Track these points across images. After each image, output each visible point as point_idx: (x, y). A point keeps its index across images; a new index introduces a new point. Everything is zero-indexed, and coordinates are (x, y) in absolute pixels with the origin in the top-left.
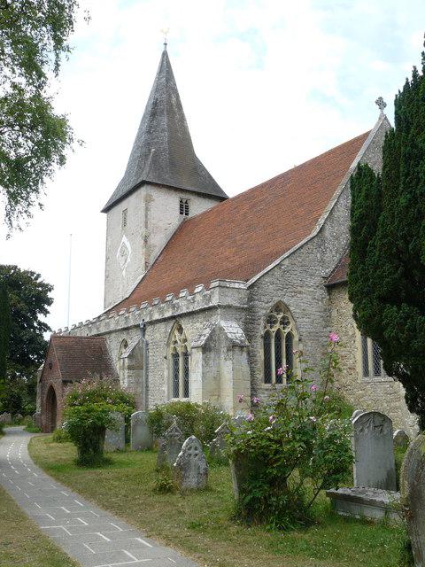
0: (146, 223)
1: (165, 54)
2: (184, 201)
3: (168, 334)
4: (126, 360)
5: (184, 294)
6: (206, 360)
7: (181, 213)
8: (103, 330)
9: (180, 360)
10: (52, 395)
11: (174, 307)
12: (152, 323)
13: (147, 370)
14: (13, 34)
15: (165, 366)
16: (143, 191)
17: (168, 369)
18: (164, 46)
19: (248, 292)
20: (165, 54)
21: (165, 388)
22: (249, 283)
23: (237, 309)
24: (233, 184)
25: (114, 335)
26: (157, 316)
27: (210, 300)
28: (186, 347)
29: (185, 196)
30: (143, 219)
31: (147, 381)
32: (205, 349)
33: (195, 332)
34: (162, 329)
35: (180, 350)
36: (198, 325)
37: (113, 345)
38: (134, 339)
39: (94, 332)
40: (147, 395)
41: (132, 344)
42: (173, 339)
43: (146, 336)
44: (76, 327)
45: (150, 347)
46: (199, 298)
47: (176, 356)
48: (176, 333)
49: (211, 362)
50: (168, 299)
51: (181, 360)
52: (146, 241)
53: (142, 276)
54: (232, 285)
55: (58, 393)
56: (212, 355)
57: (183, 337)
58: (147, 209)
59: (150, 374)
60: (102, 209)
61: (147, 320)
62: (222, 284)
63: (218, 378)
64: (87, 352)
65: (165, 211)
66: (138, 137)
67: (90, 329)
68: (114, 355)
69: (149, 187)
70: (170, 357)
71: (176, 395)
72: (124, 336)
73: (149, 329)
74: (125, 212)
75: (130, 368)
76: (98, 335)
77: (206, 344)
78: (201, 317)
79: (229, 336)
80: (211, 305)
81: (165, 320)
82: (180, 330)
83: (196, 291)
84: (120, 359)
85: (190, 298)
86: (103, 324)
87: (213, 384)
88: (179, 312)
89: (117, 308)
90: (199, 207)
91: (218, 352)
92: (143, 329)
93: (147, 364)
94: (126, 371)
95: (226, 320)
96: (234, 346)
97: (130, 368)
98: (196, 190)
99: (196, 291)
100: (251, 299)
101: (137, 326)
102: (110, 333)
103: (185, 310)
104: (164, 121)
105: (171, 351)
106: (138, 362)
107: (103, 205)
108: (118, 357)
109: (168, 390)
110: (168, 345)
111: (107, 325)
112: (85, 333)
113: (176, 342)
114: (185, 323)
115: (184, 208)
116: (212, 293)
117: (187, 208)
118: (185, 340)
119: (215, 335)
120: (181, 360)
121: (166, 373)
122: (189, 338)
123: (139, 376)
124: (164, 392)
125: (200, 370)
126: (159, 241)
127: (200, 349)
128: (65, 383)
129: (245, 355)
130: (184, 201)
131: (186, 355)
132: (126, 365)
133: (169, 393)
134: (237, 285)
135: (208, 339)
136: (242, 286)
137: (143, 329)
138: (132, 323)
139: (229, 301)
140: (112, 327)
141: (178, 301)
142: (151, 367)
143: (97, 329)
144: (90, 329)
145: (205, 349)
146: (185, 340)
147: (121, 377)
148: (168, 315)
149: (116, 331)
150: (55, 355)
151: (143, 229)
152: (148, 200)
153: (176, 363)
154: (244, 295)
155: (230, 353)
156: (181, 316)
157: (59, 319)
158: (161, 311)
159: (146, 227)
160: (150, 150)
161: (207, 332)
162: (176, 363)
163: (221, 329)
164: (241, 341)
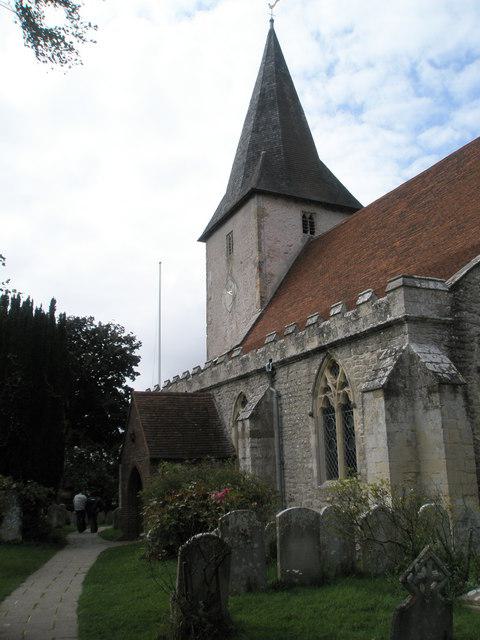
0: (259, 243)
1: (272, 34)
2: (308, 216)
3: (313, 378)
4: (248, 423)
5: (337, 311)
6: (391, 411)
7: (305, 232)
8: (208, 383)
9: (337, 422)
10: (136, 481)
11: (321, 332)
12: (286, 363)
13: (281, 436)
14: (18, 489)
15: (312, 428)
16: (253, 205)
17: (316, 432)
18: (269, 24)
19: (451, 295)
20: (272, 34)
21: (313, 465)
22: (451, 281)
23: (436, 323)
24: (365, 205)
25: (225, 389)
26: (292, 351)
27: (387, 311)
28: (346, 396)
29: (309, 209)
30: (256, 240)
31: (281, 454)
32: (389, 391)
33: (363, 368)
34: (304, 372)
35: (335, 403)
36: (367, 355)
37: (225, 401)
38: (256, 392)
39: (196, 387)
40: (282, 477)
41: (254, 399)
42: (323, 385)
43: (277, 386)
44: (169, 384)
45: (285, 399)
46: (365, 311)
47: (328, 411)
48: (327, 374)
49: (400, 415)
50: (310, 322)
51: (338, 416)
52: (260, 269)
53: (257, 316)
54: (424, 285)
55: (145, 476)
56: (401, 402)
57: (339, 378)
58: (260, 227)
59: (286, 443)
60: (199, 236)
61: (277, 358)
62: (409, 282)
63: (414, 442)
64: (188, 416)
65: (285, 225)
66: (242, 140)
67: (190, 384)
68: (227, 418)
69: (260, 198)
70: (318, 413)
71: (332, 474)
72: (241, 388)
73: (281, 373)
74: (230, 237)
75: (253, 434)
76: (202, 390)
77: (388, 383)
78: (372, 343)
79: (430, 367)
80: (389, 319)
81: (306, 356)
82: (334, 368)
83: (360, 301)
84: (236, 423)
85: (349, 314)
86: (208, 374)
87: (407, 451)
88: (332, 339)
89: (277, 294)
90: (326, 222)
91: (411, 397)
92: (271, 374)
93: (281, 428)
94: (248, 440)
95: (419, 342)
96: (443, 385)
97: (253, 434)
98: (323, 200)
99: (360, 301)
100: (456, 308)
101: (261, 372)
102: (219, 386)
103: (341, 335)
104: (276, 116)
105: (320, 404)
106: (267, 424)
107: (200, 234)
108: (235, 421)
109: (319, 468)
110: (314, 394)
111: (214, 375)
112: (183, 388)
113: (327, 389)
114: (343, 358)
115: (308, 225)
116: (393, 298)
117: (312, 225)
118: (345, 384)
119: (405, 365)
120: (338, 416)
121: (313, 441)
122: (352, 378)
123: (268, 447)
124: (311, 470)
125: (383, 429)
126: (278, 268)
127: (381, 393)
128: (155, 461)
129: (460, 398)
130: (308, 216)
131: (347, 408)
132: (247, 430)
133: (319, 473)
134: (432, 285)
135: (392, 375)
136: (440, 286)
137: (271, 374)
138: (252, 367)
139: (422, 310)
140: (223, 377)
141: (328, 322)
142: (287, 430)
143: (201, 382)
144: (190, 384)
145: (389, 391)
146: (345, 384)
147: (240, 457)
148: (310, 347)
149: (228, 382)
150: (139, 421)
151: (256, 253)
152: (261, 215)
153: (329, 424)
154: (445, 300)
155: (436, 398)
156: (335, 345)
157: (144, 380)
158: (300, 342)
159: (260, 250)
160: (259, 153)
161: (389, 363)
162: (329, 424)
163: (412, 357)
164: (451, 375)
